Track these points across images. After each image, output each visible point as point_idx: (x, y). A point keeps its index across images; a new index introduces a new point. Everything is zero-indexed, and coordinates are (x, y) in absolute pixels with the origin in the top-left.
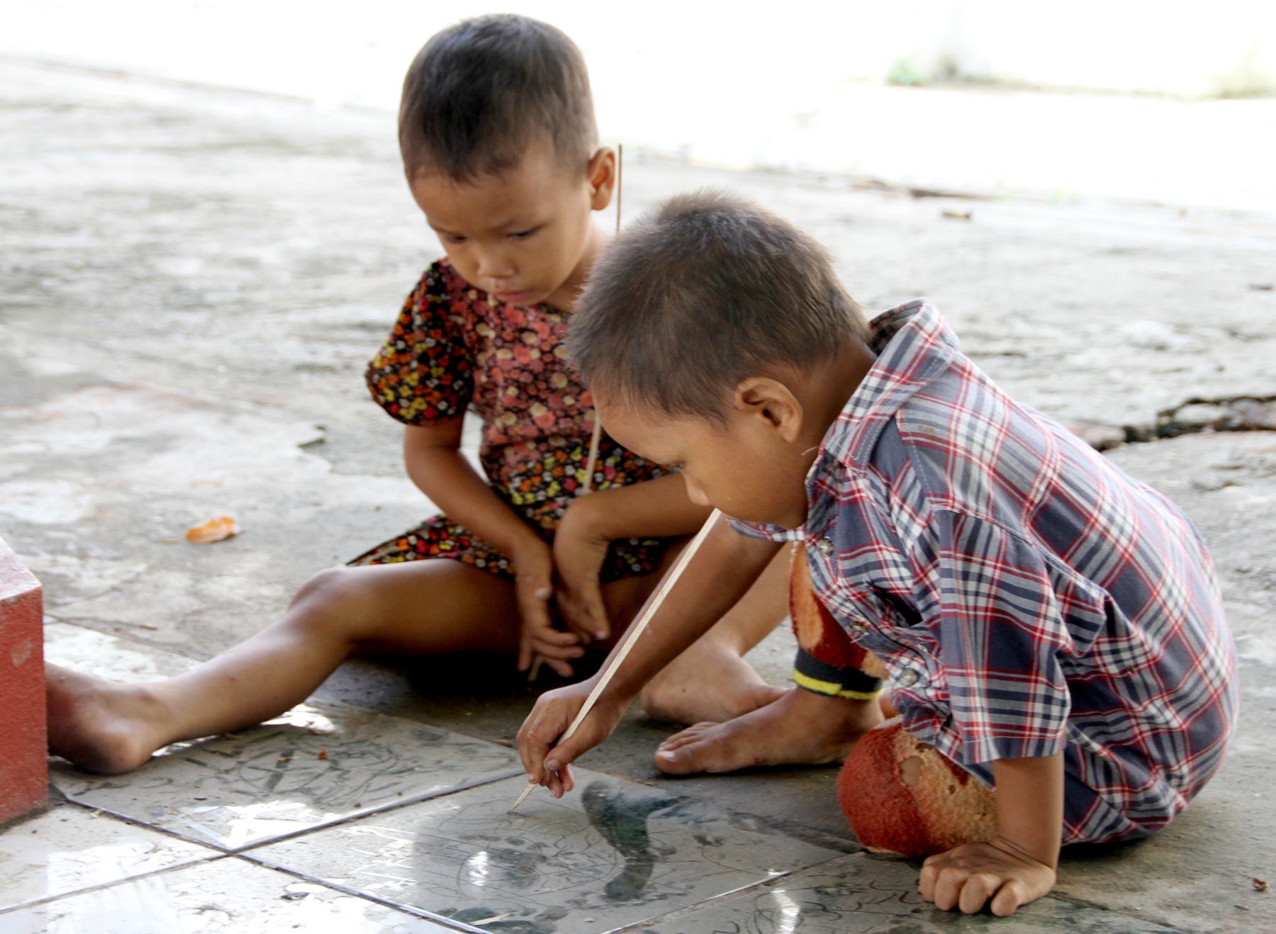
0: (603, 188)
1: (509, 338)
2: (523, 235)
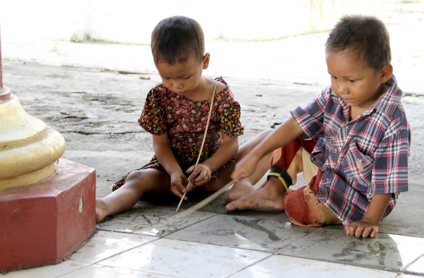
0: (206, 63)
1: (178, 107)
2: (188, 78)
